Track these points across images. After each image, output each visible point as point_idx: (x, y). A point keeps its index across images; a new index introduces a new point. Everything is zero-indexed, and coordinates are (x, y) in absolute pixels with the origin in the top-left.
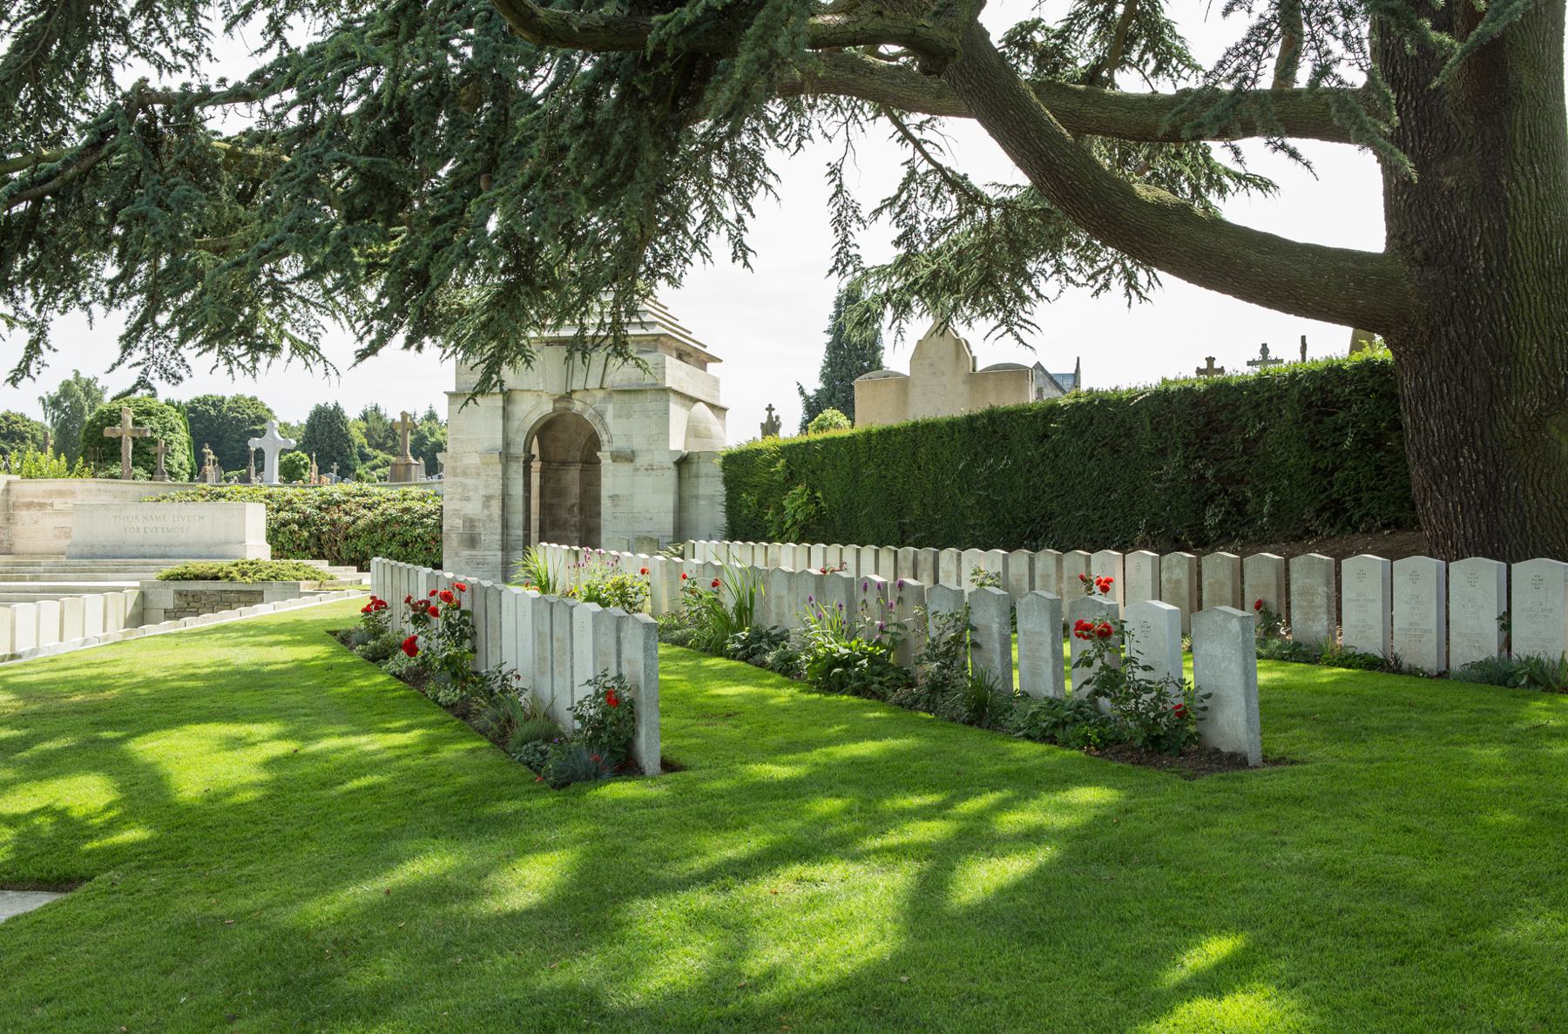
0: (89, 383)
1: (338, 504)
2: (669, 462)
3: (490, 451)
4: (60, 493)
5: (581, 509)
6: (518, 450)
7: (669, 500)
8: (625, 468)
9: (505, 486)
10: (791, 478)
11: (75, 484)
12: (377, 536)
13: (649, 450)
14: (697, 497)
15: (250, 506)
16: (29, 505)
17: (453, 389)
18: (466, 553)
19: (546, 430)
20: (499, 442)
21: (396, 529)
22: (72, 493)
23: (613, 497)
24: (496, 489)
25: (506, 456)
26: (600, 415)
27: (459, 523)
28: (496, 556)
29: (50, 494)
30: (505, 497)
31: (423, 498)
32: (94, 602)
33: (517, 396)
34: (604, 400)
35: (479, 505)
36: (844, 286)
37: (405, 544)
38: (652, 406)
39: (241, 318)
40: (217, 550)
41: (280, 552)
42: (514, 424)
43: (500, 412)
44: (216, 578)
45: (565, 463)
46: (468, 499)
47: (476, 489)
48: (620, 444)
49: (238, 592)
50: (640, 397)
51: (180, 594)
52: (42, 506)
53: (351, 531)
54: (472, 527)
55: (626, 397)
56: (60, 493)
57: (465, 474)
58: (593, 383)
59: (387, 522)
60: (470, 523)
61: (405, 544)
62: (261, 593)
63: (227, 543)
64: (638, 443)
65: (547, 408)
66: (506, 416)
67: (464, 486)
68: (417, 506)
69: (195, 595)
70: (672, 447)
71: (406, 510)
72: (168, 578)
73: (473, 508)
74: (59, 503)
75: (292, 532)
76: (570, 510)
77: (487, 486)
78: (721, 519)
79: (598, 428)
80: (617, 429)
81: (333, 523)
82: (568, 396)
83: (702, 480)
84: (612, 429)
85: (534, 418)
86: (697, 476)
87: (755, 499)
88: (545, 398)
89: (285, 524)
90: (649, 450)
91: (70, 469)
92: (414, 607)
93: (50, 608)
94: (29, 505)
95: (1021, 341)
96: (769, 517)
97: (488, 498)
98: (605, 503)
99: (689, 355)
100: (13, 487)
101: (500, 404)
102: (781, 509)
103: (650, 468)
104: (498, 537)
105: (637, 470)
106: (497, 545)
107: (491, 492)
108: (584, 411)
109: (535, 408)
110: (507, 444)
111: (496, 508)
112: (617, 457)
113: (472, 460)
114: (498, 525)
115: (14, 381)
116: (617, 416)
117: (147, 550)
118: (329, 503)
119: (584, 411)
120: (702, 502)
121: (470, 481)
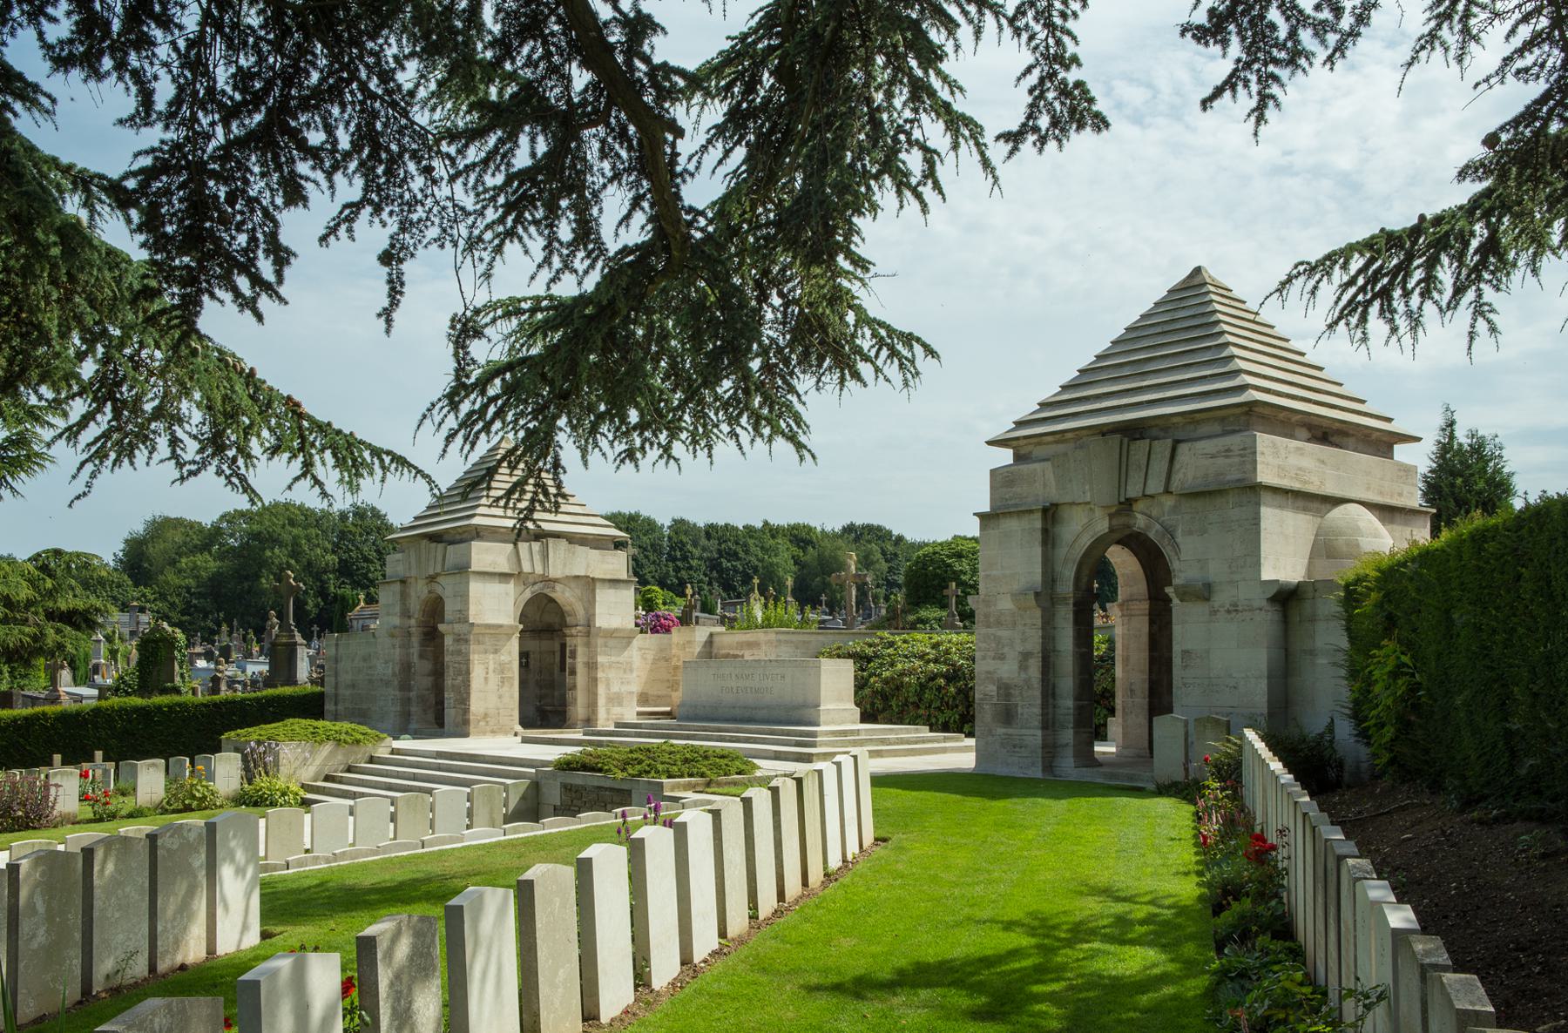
6: (1066, 587)
13: (1231, 582)
15: (827, 665)
17: (986, 508)
18: (1001, 731)
24: (1034, 643)
26: (1169, 532)
27: (992, 689)
28: (1034, 736)
29: (742, 645)
33: (1065, 513)
34: (1175, 510)
35: (1016, 667)
36: (725, 109)
42: (1061, 552)
43: (1039, 536)
46: (1002, 657)
49: (611, 789)
52: (736, 656)
54: (1008, 695)
55: (1198, 504)
57: (999, 623)
58: (1155, 486)
60: (1005, 689)
62: (629, 792)
64: (1216, 571)
67: (998, 640)
70: (1266, 575)
73: (1008, 670)
75: (939, 688)
77: (1024, 640)
82: (1127, 505)
86: (1313, 619)
88: (1098, 513)
89: (933, 677)
90: (1231, 582)
95: (1024, 75)
97: (1026, 656)
98: (1177, 660)
99: (1345, 434)
100: (716, 639)
101: (1038, 524)
103: (1234, 609)
104: (1037, 710)
105: (1214, 612)
106: (1036, 722)
108: (1148, 527)
109: (1086, 527)
113: (1006, 604)
114: (1038, 693)
119: (1148, 527)
120: (1322, 661)
121: (1004, 633)
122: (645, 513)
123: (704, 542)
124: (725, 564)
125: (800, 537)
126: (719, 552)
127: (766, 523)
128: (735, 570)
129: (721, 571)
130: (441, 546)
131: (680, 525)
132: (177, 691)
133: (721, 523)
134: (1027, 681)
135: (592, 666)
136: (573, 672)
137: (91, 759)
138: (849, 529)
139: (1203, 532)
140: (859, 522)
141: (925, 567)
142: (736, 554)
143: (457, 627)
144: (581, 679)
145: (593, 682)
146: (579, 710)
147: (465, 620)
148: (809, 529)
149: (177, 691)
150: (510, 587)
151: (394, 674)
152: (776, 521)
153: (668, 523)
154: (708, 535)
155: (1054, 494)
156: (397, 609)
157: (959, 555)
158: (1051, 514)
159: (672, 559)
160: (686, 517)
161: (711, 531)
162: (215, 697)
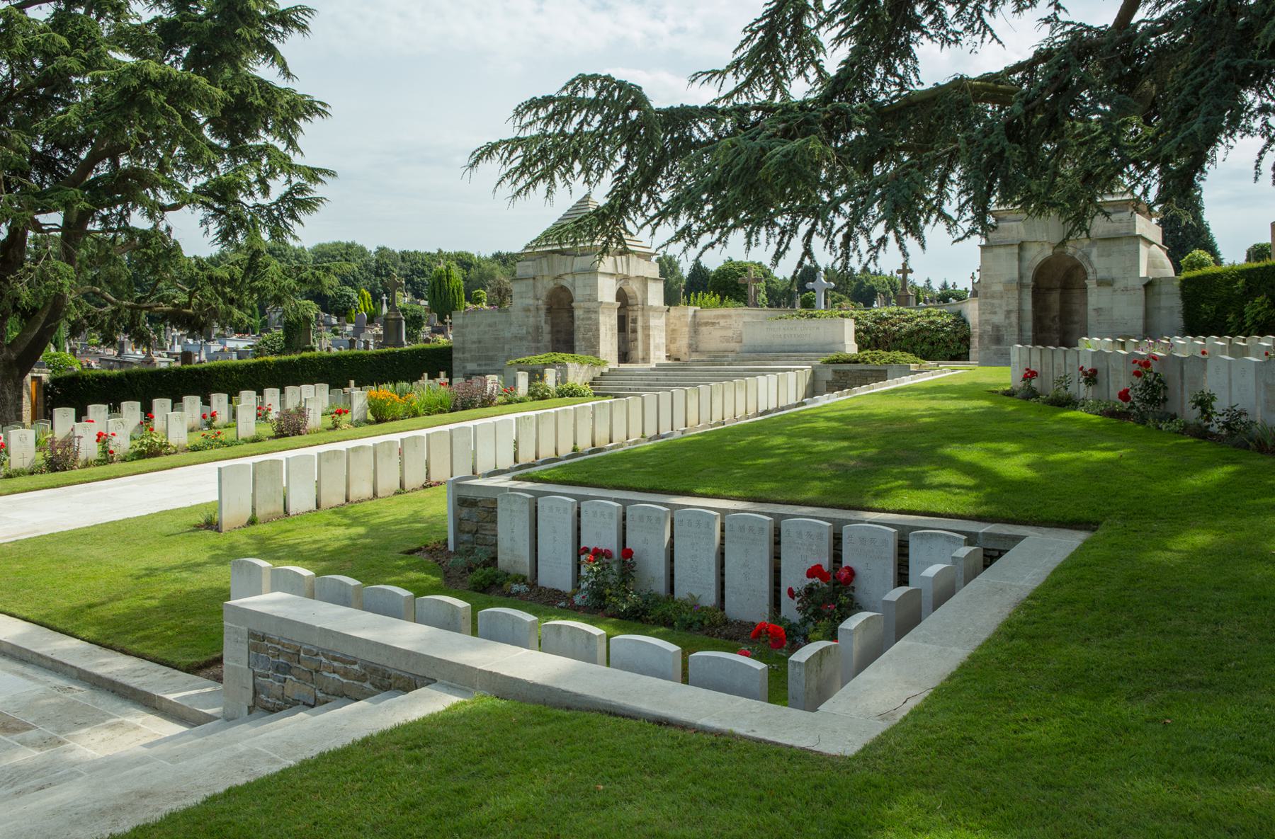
0: (671, 258)
1: (886, 319)
2: (1140, 285)
3: (1010, 282)
4: (723, 317)
5: (1060, 319)
7: (1139, 311)
8: (1107, 291)
9: (1020, 304)
10: (1250, 292)
11: (722, 311)
12: (915, 338)
14: (1159, 308)
16: (706, 324)
18: (994, 347)
19: (1042, 270)
20: (1016, 275)
21: (927, 334)
22: (730, 316)
23: (1097, 310)
24: (1014, 305)
25: (1021, 286)
26: (1087, 256)
29: (717, 317)
30: (1020, 311)
31: (940, 315)
32: (792, 375)
33: (1028, 246)
34: (1089, 246)
35: (1003, 317)
37: (932, 344)
38: (1126, 248)
39: (588, 244)
40: (828, 348)
41: (862, 346)
42: (1026, 264)
44: (856, 362)
45: (1049, 289)
46: (995, 313)
47: (1000, 306)
48: (1102, 274)
50: (1117, 242)
51: (835, 372)
52: (713, 324)
53: (897, 336)
55: (1107, 243)
56: (723, 317)
57: (993, 297)
59: (920, 330)
61: (932, 344)
63: (833, 343)
64: (1116, 272)
65: (1048, 252)
66: (1020, 259)
67: (993, 305)
68: (939, 320)
69: (845, 372)
71: (932, 322)
72: (829, 362)
74: (722, 322)
76: (1053, 320)
78: (1179, 321)
79: (1085, 264)
80: (1099, 263)
81: (885, 331)
83: (1163, 297)
84: (1096, 265)
85: (1040, 259)
86: (1159, 294)
87: (1214, 308)
88: (1046, 246)
91: (721, 303)
92: (1085, 373)
93: (772, 378)
94: (706, 324)
96: (1230, 319)
97: (1009, 312)
102: (1241, 314)
103: (1126, 289)
105: (1115, 291)
107: (1011, 308)
109: (1040, 253)
110: (1021, 277)
111: (1014, 318)
112: (1102, 283)
114: (1016, 329)
115: (1256, 179)
116: (1100, 255)
117: (786, 348)
118: (880, 319)
120: (1164, 312)
121: (996, 302)
122: (359, 243)
123: (400, 263)
124: (416, 279)
125: (464, 262)
126: (412, 271)
127: (440, 251)
128: (424, 284)
129: (413, 284)
130: (569, 258)
131: (382, 251)
132: (313, 349)
133: (412, 250)
134: (1010, 325)
135: (647, 328)
136: (634, 331)
137: (348, 385)
138: (497, 256)
139: (1109, 255)
140: (504, 251)
141: (725, 277)
142: (423, 272)
143: (587, 305)
144: (640, 335)
145: (647, 337)
146: (640, 353)
147: (595, 300)
148: (471, 256)
149: (313, 349)
150: (614, 281)
151: (528, 333)
152: (446, 250)
153: (374, 250)
154: (403, 259)
155: (1024, 236)
156: (531, 294)
157: (745, 270)
158: (1021, 246)
159: (377, 274)
160: (387, 246)
161: (404, 256)
162: (187, 367)
